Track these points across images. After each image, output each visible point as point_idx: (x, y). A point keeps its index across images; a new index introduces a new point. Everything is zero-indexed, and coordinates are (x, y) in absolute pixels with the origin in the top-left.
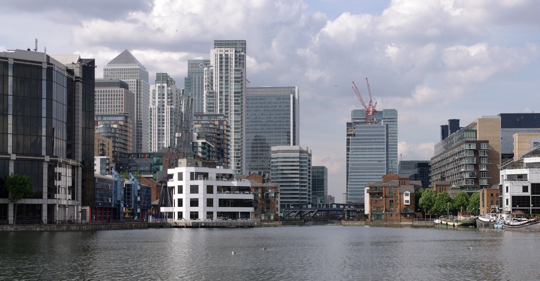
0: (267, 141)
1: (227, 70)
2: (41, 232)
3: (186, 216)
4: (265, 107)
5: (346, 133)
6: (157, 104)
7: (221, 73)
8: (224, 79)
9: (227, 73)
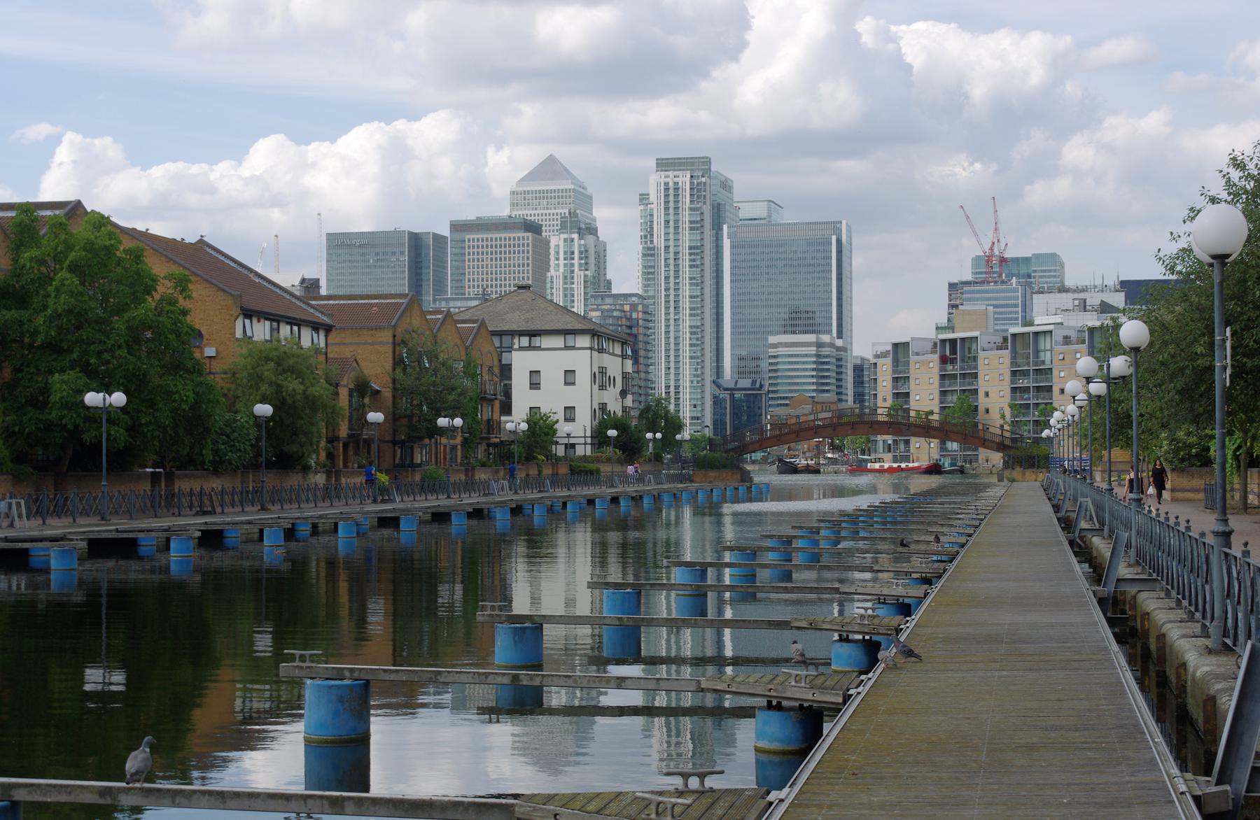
0: (817, 321)
1: (676, 208)
4: (785, 259)
5: (947, 302)
6: (562, 269)
7: (667, 214)
8: (671, 224)
9: (676, 214)
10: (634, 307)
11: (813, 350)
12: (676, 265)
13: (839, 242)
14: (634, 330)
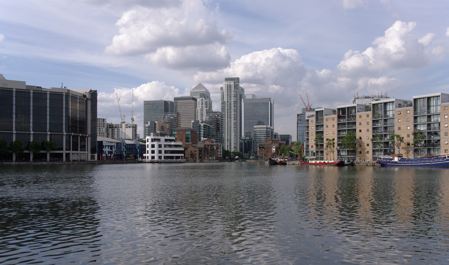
1: (230, 91)
2: (62, 164)
3: (150, 158)
10: (218, 115)
11: (265, 129)
12: (230, 106)
13: (271, 103)
14: (218, 122)
